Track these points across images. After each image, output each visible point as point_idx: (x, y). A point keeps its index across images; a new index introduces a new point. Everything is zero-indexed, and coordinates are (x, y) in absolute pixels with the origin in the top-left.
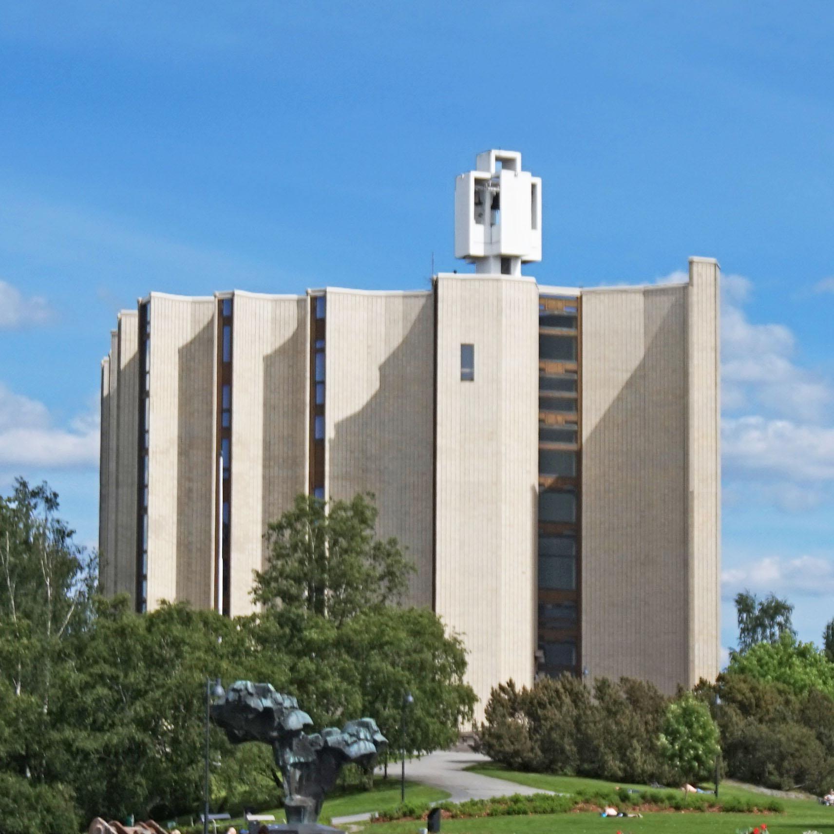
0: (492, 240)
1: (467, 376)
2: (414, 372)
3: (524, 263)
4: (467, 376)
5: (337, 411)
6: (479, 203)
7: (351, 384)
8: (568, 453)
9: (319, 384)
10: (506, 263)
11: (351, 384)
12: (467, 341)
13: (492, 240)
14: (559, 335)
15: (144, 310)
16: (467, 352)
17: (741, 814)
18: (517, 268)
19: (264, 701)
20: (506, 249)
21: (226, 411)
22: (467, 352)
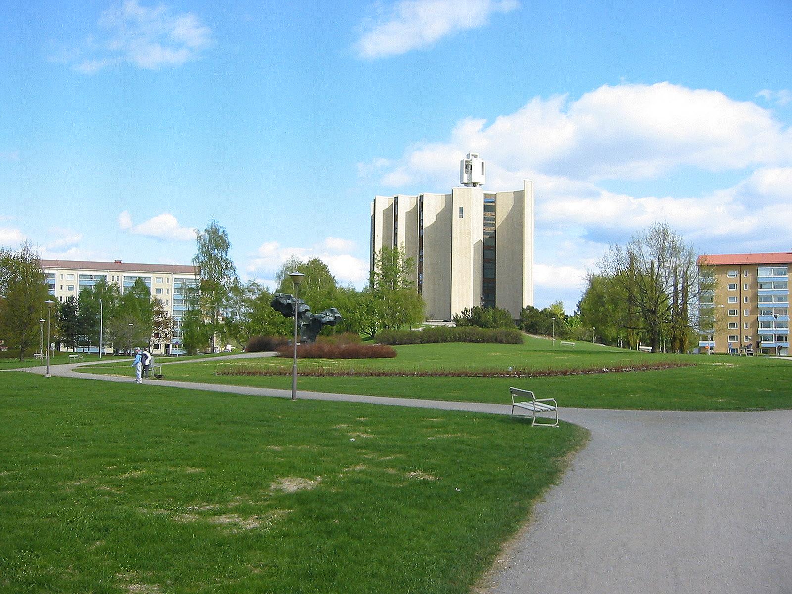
0: (470, 178)
1: (462, 217)
2: (446, 218)
3: (480, 185)
4: (462, 217)
5: (426, 224)
6: (466, 168)
7: (429, 218)
8: (293, 354)
9: (421, 220)
10: (475, 185)
11: (429, 218)
12: (462, 206)
13: (470, 178)
14: (156, 507)
15: (375, 200)
16: (461, 210)
17: (513, 345)
18: (478, 186)
19: (288, 301)
20: (474, 180)
21: (396, 228)
22: (461, 210)
